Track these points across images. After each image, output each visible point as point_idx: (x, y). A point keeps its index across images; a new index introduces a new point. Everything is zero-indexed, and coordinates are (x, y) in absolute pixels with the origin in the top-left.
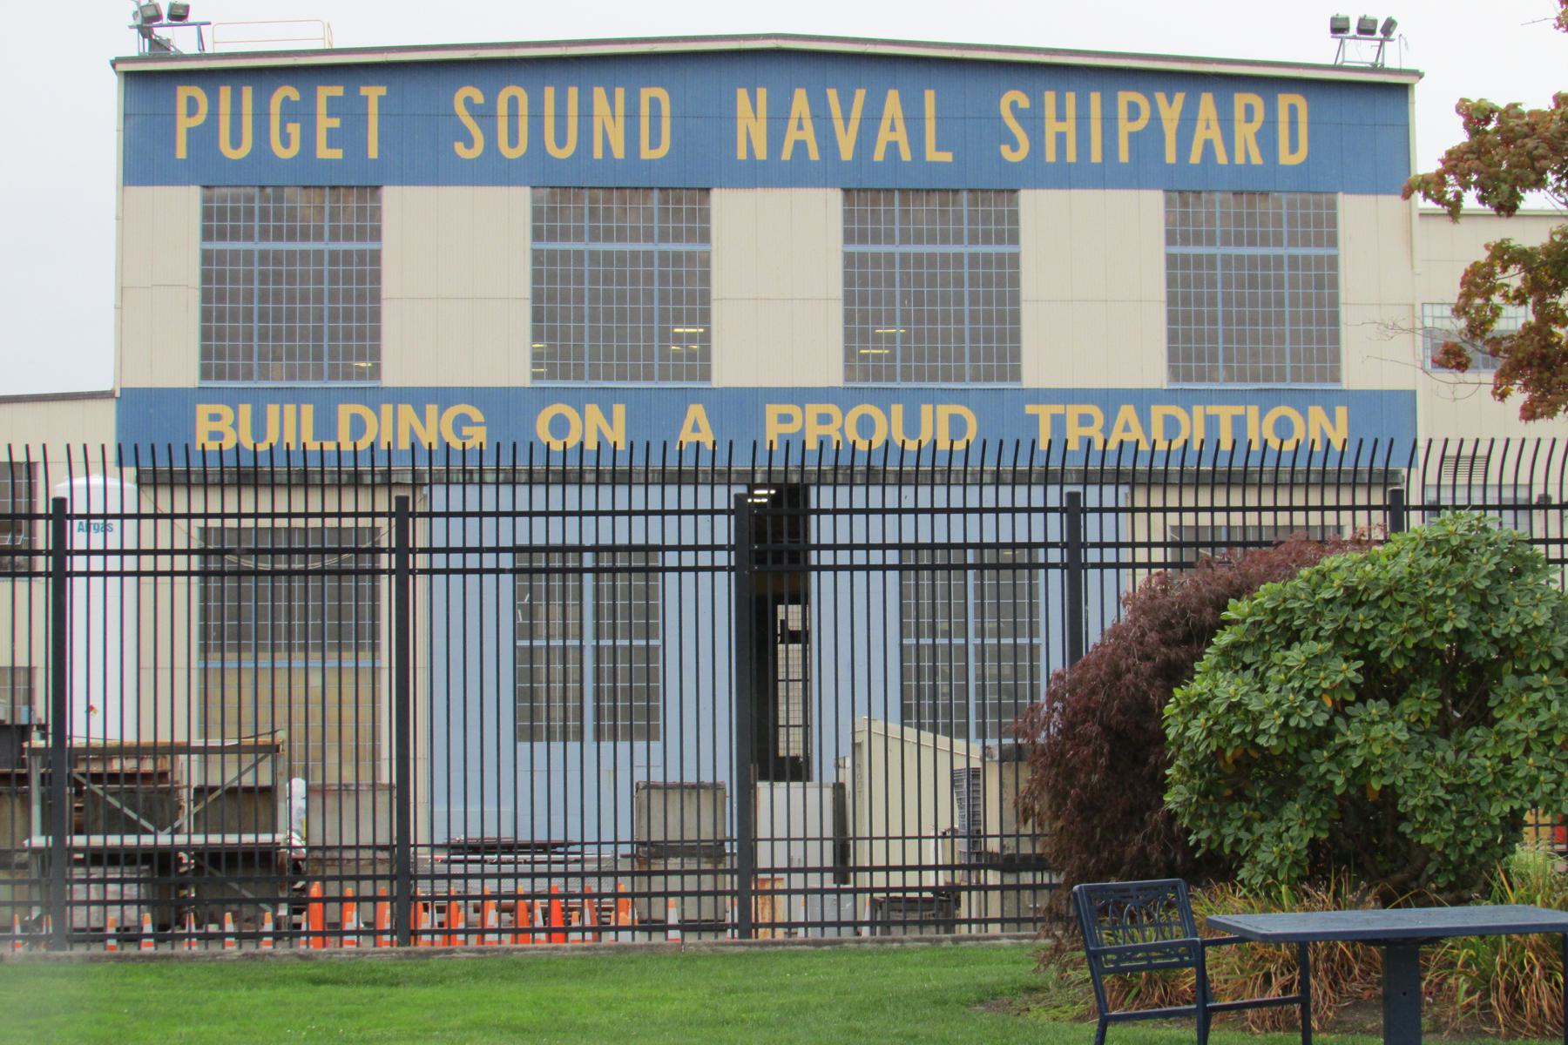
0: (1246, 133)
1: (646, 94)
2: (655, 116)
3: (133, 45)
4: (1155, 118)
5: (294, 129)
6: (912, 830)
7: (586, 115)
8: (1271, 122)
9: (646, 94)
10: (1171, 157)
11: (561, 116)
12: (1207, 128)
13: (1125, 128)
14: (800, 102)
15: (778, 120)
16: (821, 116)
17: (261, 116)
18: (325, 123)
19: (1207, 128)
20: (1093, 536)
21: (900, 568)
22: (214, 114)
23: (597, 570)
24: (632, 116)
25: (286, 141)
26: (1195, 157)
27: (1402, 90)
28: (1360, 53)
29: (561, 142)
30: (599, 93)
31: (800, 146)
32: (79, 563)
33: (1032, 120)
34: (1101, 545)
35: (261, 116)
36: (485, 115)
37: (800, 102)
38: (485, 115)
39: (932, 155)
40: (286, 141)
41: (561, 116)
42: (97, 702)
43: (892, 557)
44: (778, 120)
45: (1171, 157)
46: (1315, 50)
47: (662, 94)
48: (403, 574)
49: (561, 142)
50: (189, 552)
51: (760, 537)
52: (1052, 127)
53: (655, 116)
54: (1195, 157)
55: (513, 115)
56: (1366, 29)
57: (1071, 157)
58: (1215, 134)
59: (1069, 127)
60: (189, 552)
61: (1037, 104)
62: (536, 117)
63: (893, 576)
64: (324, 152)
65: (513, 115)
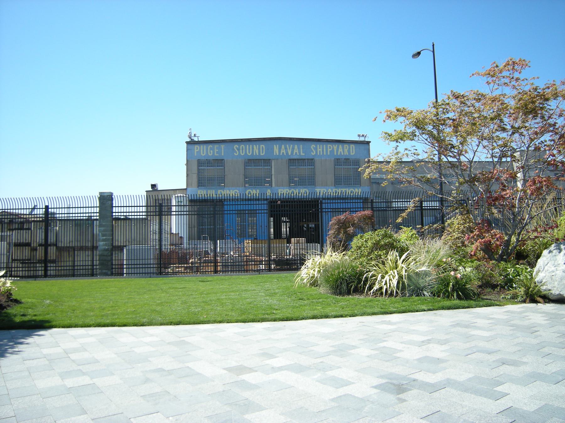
0: (346, 150)
1: (261, 146)
2: (263, 149)
3: (189, 140)
4: (333, 148)
5: (212, 151)
6: (133, 258)
7: (253, 149)
8: (349, 149)
9: (261, 146)
10: (335, 154)
11: (249, 149)
12: (340, 150)
13: (329, 150)
14: (296, 147)
15: (280, 149)
16: (286, 148)
17: (207, 149)
18: (216, 150)
19: (340, 150)
20: (163, 210)
21: (189, 215)
22: (200, 149)
23: (248, 213)
24: (259, 149)
25: (210, 153)
26: (339, 154)
27: (368, 143)
28: (362, 139)
29: (249, 153)
30: (255, 146)
31: (283, 153)
32: (324, 210)
33: (316, 149)
34: (325, 209)
35: (207, 149)
36: (238, 149)
37: (296, 147)
38: (238, 149)
39: (302, 154)
40: (210, 153)
41: (249, 149)
42: (260, 228)
43: (188, 213)
44: (280, 149)
45: (335, 154)
46: (357, 139)
47: (264, 146)
48: (322, 212)
49: (249, 153)
50: (186, 211)
51: (272, 208)
52: (319, 150)
53: (263, 149)
54: (339, 154)
55: (242, 149)
56: (363, 136)
57: (325, 154)
58: (342, 150)
59: (321, 150)
60: (186, 211)
61: (316, 147)
62: (246, 149)
63: (196, 216)
64: (216, 154)
65: (242, 149)
